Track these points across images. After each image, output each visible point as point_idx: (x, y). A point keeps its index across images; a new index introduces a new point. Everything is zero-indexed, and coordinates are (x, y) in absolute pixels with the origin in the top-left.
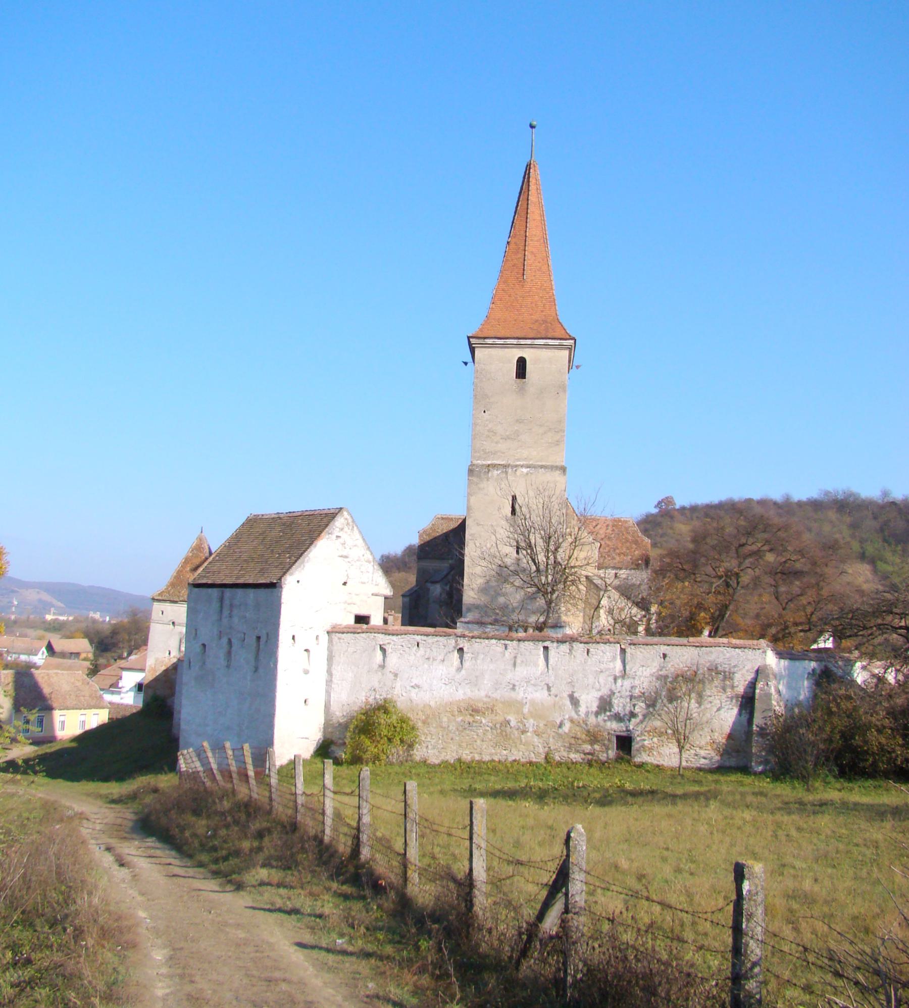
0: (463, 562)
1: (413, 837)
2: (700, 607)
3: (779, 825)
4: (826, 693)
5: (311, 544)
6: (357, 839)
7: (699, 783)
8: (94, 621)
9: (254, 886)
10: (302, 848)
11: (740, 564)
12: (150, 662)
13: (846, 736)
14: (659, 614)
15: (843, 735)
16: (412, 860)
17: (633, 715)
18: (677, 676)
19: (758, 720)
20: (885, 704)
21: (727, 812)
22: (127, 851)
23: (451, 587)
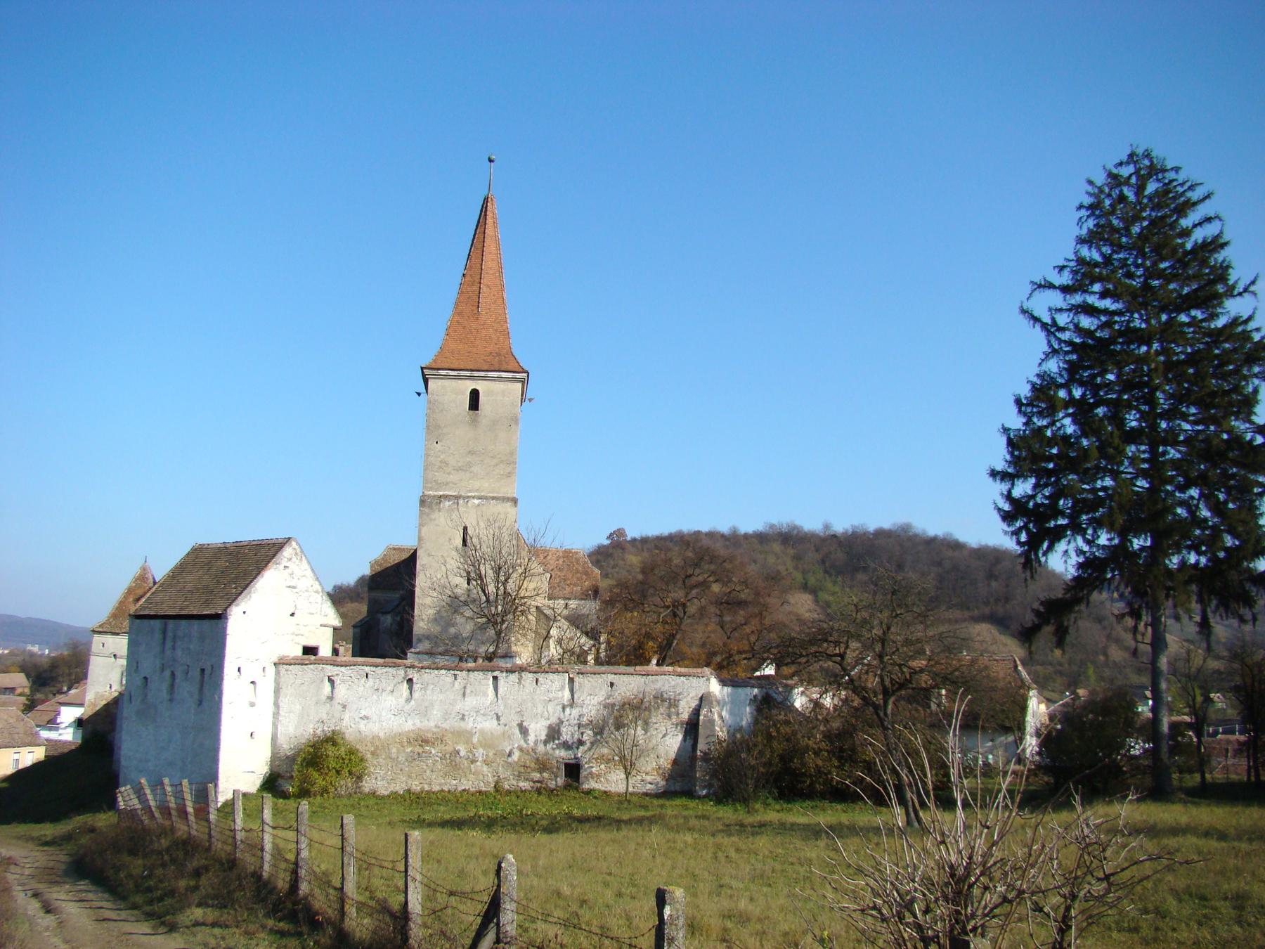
0: (413, 592)
1: (351, 871)
2: (648, 636)
3: (718, 847)
4: (766, 718)
5: (258, 574)
6: (295, 872)
7: (645, 807)
8: (32, 655)
9: (187, 927)
10: (240, 885)
11: (687, 594)
12: (90, 696)
13: (785, 758)
14: (608, 642)
15: (782, 757)
16: (350, 894)
17: (581, 743)
18: (624, 704)
19: (702, 746)
20: (822, 728)
21: (669, 835)
22: (55, 896)
23: (402, 618)
